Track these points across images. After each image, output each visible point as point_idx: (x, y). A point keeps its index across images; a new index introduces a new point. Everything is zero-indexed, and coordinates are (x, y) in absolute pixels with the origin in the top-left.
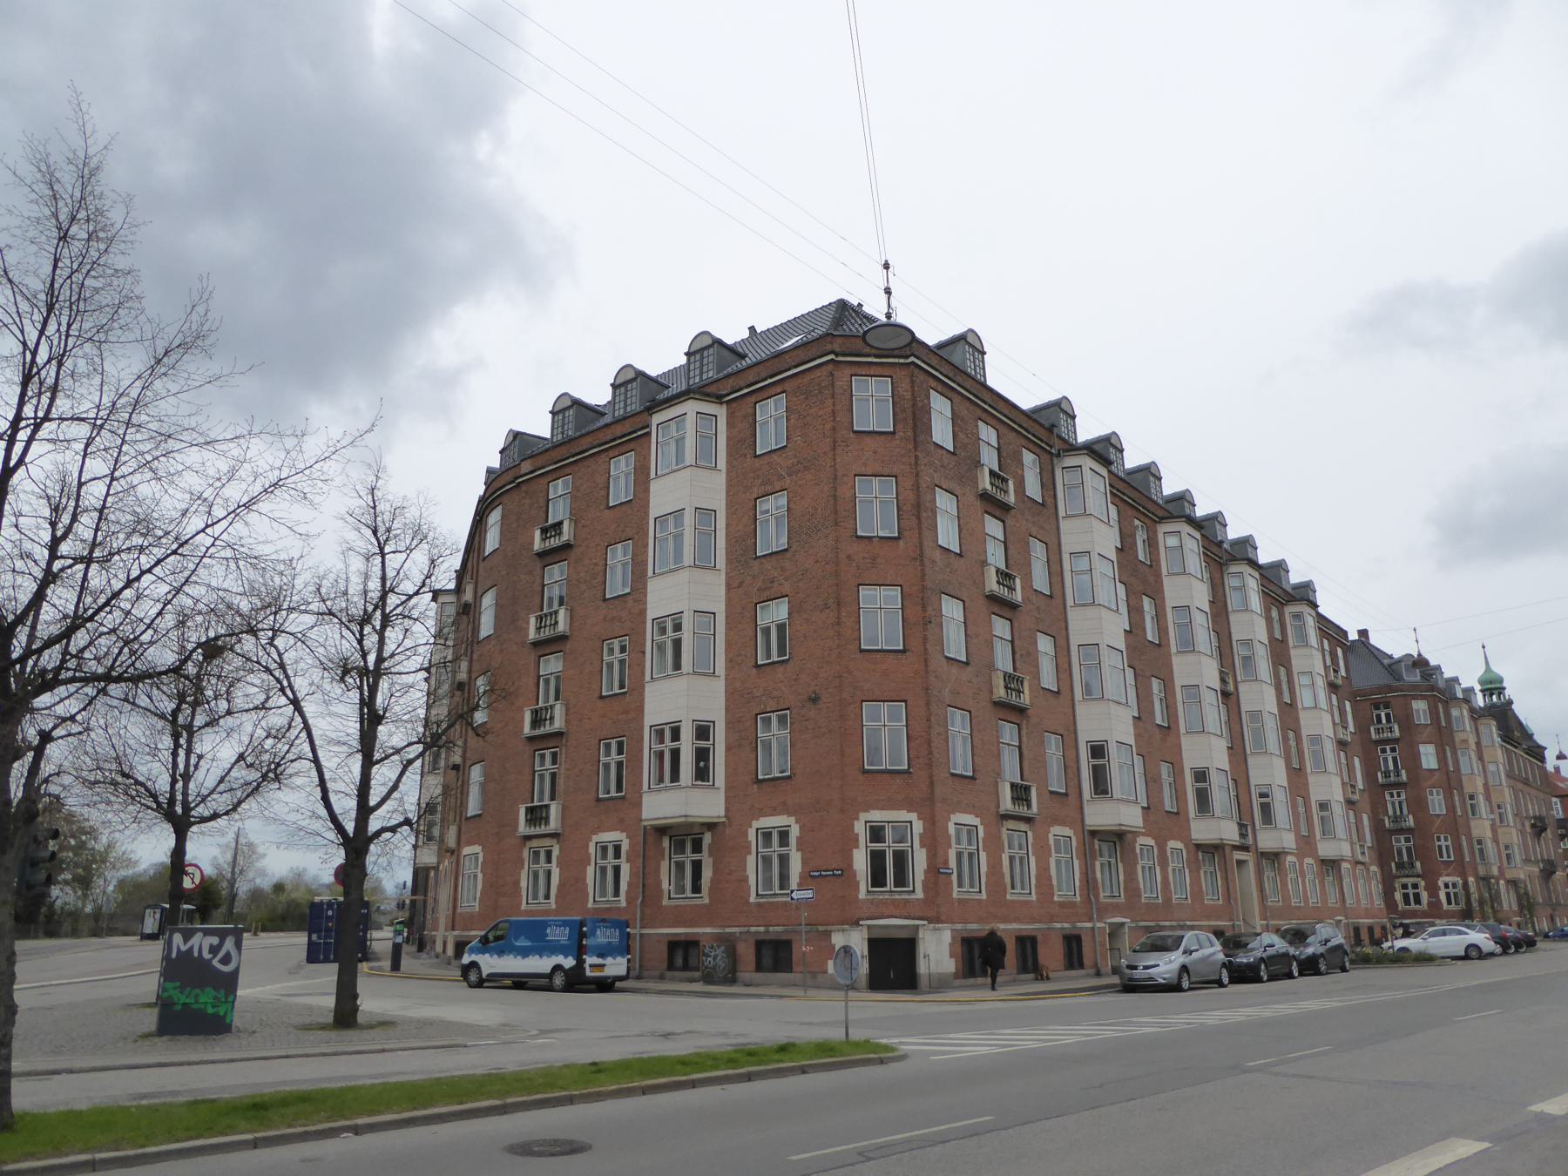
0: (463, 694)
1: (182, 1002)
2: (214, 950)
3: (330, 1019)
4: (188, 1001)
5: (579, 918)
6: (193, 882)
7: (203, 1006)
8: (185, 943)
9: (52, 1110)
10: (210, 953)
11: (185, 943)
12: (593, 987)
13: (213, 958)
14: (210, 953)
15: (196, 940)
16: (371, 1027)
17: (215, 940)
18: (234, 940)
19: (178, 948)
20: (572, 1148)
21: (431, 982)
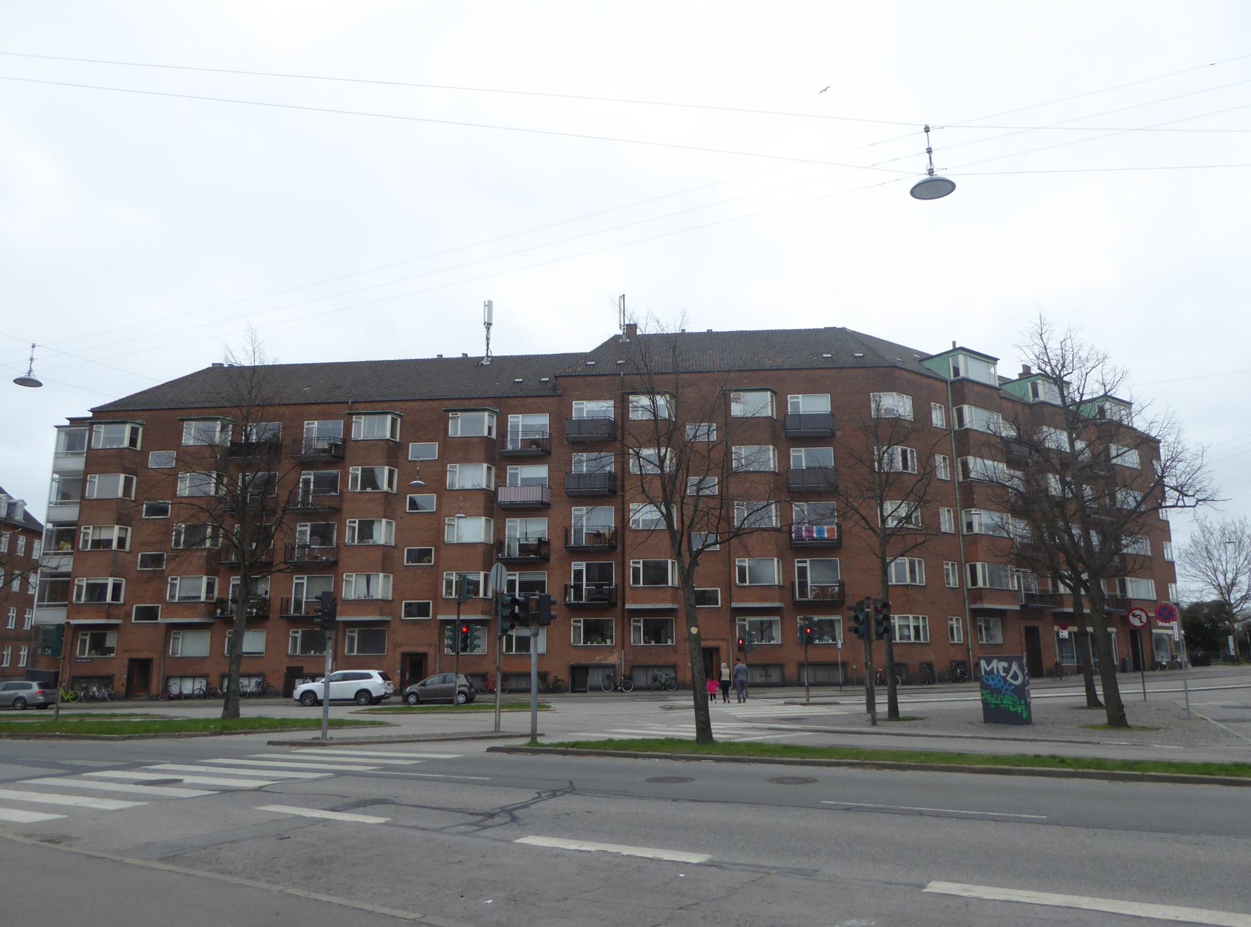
0: (958, 481)
1: (993, 702)
2: (1007, 670)
3: (887, 717)
4: (997, 702)
5: (53, 671)
6: (1141, 622)
7: (1007, 706)
8: (988, 666)
9: (1197, 762)
10: (1004, 672)
11: (988, 666)
12: (35, 707)
13: (1007, 676)
14: (1004, 672)
15: (994, 664)
16: (905, 719)
17: (1006, 664)
18: (1017, 664)
19: (985, 669)
20: (814, 781)
21: (1244, 689)
